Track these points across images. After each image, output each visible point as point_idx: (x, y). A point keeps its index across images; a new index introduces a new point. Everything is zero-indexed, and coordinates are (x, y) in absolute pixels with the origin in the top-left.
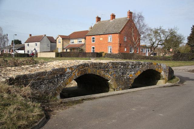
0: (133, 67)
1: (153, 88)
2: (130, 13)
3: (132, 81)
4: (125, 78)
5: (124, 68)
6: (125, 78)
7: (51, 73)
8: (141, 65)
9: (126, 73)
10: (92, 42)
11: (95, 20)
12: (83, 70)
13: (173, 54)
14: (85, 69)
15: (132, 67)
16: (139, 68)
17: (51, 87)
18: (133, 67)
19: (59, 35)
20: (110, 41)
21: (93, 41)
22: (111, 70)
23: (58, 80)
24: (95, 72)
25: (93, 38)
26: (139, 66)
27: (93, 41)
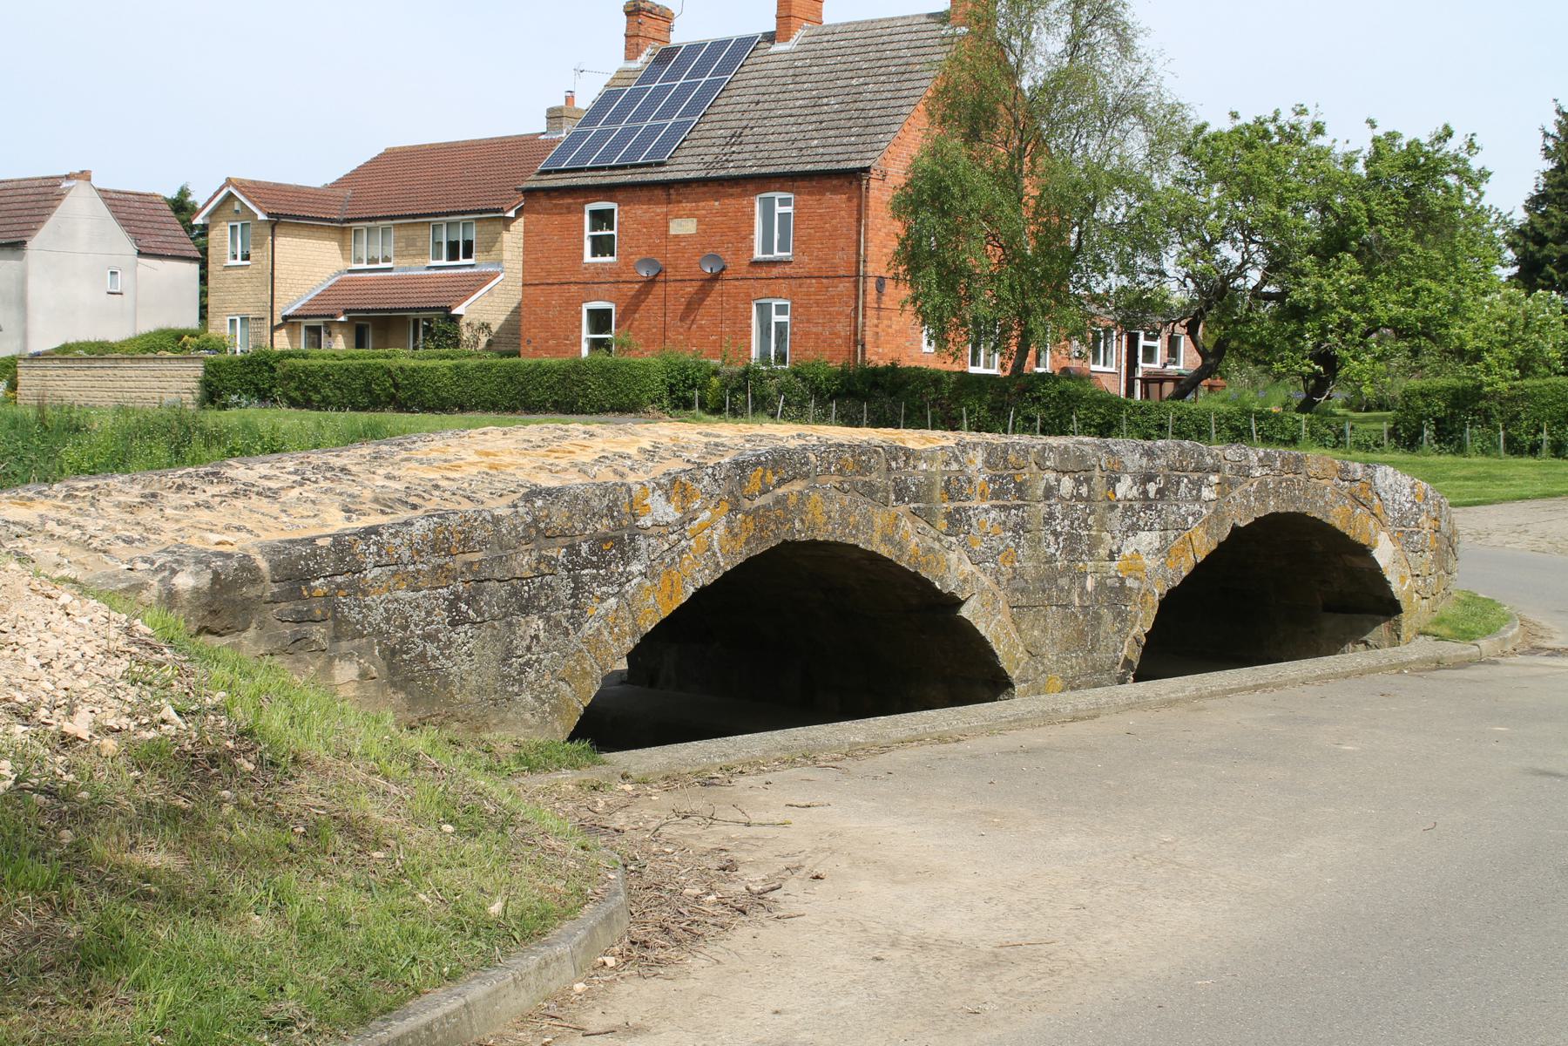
0: (1152, 488)
1: (1318, 678)
2: (1490, 174)
3: (1143, 621)
4: (1090, 584)
5: (1079, 498)
6: (1090, 584)
7: (528, 526)
8: (1214, 478)
9: (1095, 543)
10: (588, 257)
11: (1229, 117)
12: (767, 508)
13: (1515, 270)
14: (782, 501)
15: (1145, 492)
16: (1198, 499)
17: (529, 649)
18: (1152, 488)
19: (229, 182)
20: (758, 254)
21: (601, 246)
22: (983, 512)
23: (578, 588)
24: (856, 527)
25: (601, 218)
26: (1197, 485)
27: (601, 246)
